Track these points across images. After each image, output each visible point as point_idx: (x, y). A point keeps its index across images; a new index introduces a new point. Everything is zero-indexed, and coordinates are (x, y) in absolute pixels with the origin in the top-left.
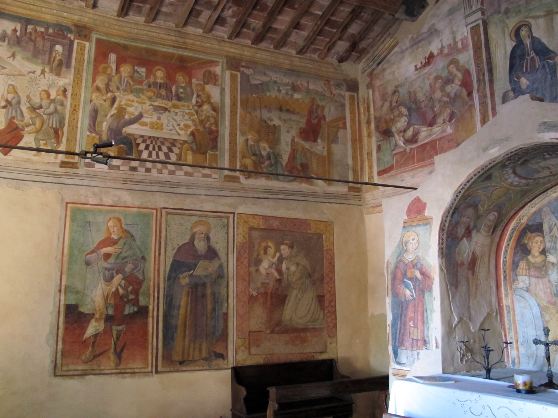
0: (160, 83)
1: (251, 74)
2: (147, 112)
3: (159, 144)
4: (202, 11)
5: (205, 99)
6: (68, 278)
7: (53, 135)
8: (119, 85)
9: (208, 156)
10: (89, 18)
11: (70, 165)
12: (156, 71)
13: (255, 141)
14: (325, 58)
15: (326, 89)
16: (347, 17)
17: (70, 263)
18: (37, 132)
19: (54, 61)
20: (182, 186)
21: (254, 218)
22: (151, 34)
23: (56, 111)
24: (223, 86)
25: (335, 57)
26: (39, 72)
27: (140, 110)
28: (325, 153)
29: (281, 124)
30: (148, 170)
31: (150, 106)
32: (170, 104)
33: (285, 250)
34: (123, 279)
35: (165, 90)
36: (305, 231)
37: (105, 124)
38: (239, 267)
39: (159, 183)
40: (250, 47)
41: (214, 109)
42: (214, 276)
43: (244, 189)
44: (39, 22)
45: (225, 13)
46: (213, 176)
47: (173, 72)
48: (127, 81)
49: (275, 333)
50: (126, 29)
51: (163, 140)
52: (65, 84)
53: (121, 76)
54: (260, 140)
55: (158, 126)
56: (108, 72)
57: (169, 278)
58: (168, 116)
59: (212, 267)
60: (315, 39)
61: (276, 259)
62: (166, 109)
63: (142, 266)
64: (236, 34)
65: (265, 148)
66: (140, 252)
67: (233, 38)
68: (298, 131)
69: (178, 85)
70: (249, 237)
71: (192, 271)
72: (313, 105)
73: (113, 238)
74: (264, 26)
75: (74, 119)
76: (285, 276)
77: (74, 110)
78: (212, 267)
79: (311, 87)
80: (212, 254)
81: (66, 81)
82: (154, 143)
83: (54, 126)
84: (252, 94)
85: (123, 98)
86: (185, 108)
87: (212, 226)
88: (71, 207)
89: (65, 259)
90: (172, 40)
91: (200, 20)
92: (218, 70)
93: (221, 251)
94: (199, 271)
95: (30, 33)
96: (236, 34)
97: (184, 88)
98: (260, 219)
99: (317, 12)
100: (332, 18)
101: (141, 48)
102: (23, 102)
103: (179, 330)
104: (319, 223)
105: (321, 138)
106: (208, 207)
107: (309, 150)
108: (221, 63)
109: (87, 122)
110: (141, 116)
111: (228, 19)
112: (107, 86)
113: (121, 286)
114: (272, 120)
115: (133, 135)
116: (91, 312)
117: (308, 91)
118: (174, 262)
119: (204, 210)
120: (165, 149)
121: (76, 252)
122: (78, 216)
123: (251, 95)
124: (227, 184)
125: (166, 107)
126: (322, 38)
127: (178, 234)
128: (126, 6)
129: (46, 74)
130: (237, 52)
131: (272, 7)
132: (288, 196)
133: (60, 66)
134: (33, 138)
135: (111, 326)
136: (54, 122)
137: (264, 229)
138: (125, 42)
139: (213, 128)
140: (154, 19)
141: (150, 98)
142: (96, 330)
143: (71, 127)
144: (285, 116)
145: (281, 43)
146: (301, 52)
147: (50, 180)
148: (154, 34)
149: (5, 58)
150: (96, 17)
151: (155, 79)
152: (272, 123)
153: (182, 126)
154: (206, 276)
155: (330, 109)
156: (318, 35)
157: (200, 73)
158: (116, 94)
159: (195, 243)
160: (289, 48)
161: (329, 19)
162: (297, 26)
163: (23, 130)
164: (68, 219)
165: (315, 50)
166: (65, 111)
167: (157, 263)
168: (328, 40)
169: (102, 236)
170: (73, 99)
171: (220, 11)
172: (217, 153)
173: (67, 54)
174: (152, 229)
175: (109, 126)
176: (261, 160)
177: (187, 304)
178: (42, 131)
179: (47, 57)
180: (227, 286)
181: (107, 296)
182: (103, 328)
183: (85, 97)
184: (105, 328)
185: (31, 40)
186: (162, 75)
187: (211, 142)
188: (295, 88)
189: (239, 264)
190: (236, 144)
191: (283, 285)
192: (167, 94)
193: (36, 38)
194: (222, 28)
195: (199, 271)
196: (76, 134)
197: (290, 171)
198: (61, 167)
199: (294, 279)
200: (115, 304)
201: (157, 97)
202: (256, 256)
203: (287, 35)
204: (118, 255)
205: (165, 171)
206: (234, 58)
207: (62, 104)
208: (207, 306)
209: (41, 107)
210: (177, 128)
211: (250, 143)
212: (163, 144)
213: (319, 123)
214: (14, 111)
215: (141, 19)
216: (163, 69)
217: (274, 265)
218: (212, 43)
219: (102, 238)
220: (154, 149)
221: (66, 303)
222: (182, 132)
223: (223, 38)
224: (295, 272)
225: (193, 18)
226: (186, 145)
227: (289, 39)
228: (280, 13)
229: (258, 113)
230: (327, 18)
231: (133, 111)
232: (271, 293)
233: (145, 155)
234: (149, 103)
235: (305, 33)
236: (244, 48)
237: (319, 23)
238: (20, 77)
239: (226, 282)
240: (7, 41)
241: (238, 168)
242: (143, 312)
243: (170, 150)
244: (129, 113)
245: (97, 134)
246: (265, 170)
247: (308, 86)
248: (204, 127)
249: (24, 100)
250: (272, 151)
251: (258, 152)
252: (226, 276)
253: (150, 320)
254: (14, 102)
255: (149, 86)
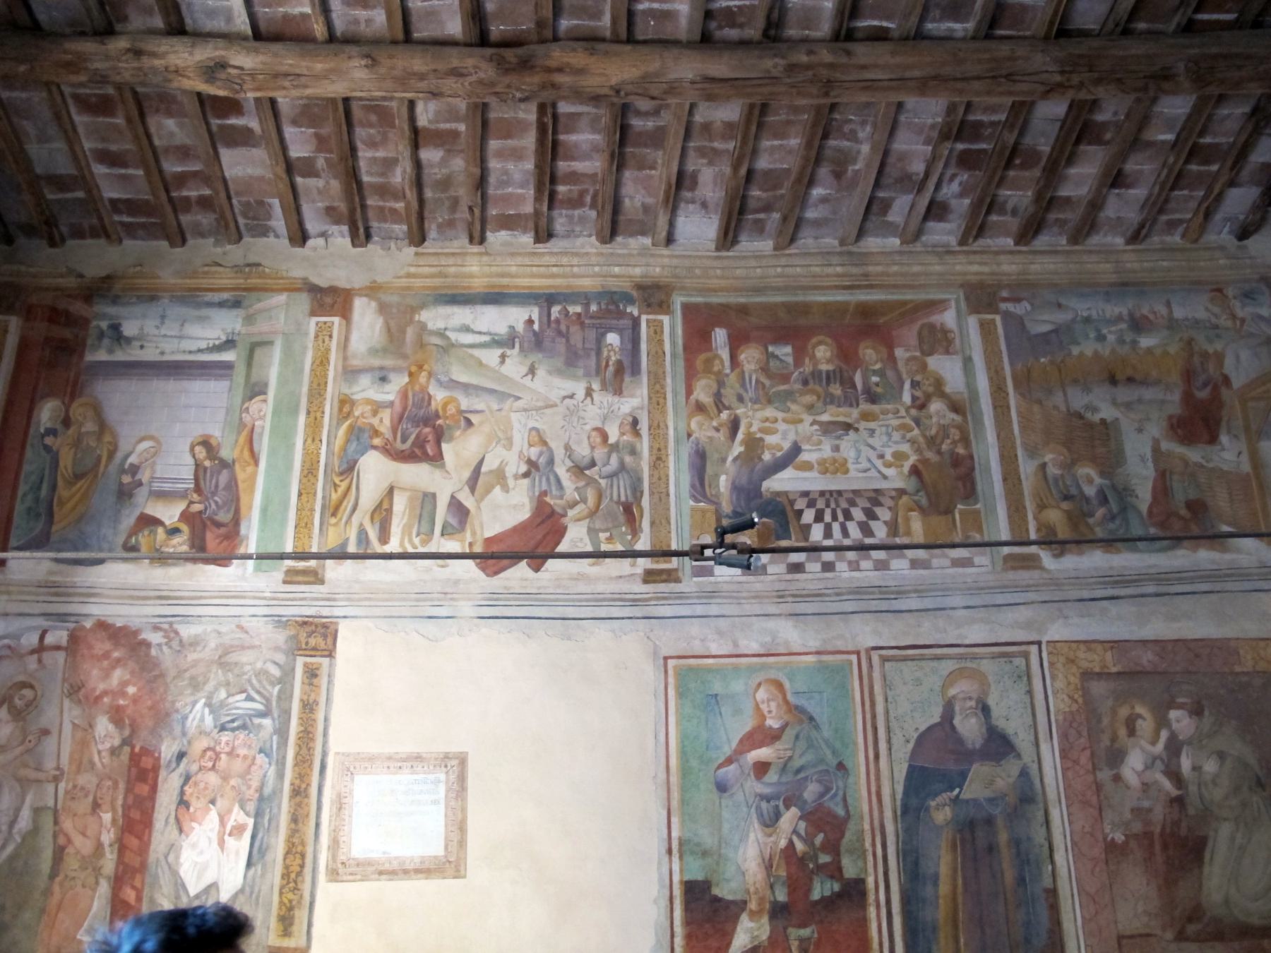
0: (828, 372)
1: (1027, 313)
2: (808, 439)
3: (844, 505)
4: (893, 199)
5: (931, 389)
6: (683, 822)
7: (622, 518)
8: (741, 391)
9: (957, 516)
10: (663, 267)
11: (664, 577)
12: (814, 347)
13: (1063, 466)
14: (1200, 236)
15: (1216, 310)
16: (1242, 128)
17: (683, 789)
18: (592, 514)
19: (607, 365)
20: (909, 592)
21: (1089, 649)
22: (789, 271)
23: (623, 466)
24: (968, 353)
25: (1226, 229)
26: (581, 393)
27: (792, 437)
28: (1246, 467)
29: (1119, 415)
30: (828, 567)
31: (812, 424)
32: (855, 413)
33: (1180, 720)
34: (800, 818)
35: (840, 384)
36: (1226, 670)
37: (723, 478)
38: (1070, 774)
39: (858, 593)
40: (1011, 252)
41: (956, 407)
42: (1012, 799)
43: (1055, 583)
44: (573, 294)
45: (944, 190)
46: (977, 560)
47: (849, 343)
48: (757, 381)
49: (1187, 939)
50: (738, 272)
51: (851, 495)
52: (634, 409)
53: (743, 372)
54: (1073, 463)
55: (836, 467)
56: (716, 369)
57: (906, 809)
58: (856, 442)
59: (1004, 776)
60: (1166, 201)
61: (1160, 747)
62: (848, 427)
63: (841, 784)
64: (976, 229)
65: (1089, 479)
66: (834, 753)
67: (971, 240)
68: (1164, 424)
69: (867, 369)
70: (1083, 696)
71: (957, 790)
72: (1191, 355)
73: (771, 728)
74: (1038, 197)
75: (660, 479)
76: (1193, 789)
77: (659, 460)
78: (1004, 776)
79: (1178, 313)
80: (998, 745)
81: (635, 402)
82: (833, 505)
83: (623, 499)
84: (1037, 359)
85: (753, 418)
86: (890, 416)
87: (990, 678)
88: (675, 667)
89: (674, 779)
90: (838, 275)
91: (890, 218)
92: (948, 318)
93: (1022, 735)
94: (973, 790)
95: (558, 321)
96: (976, 229)
97: (881, 373)
98: (1105, 651)
99: (1162, 137)
100: (1202, 140)
101: (776, 305)
102: (557, 460)
103: (942, 935)
104: (1262, 644)
105: (1229, 432)
106: (976, 634)
107: (1202, 466)
108: (953, 303)
109: (686, 479)
110: (796, 450)
111: (953, 202)
112: (718, 397)
113: (799, 836)
114: (1095, 410)
115: (786, 493)
116: (738, 897)
117: (1172, 325)
118: (912, 769)
119: (967, 642)
120: (858, 514)
121: (694, 763)
122: (691, 682)
123: (1037, 363)
124: (1011, 575)
125: (848, 420)
126: (1185, 192)
127: (914, 705)
128: (733, 225)
129: (595, 395)
130: (986, 269)
131: (1051, 154)
132: (1165, 587)
133: (618, 376)
134: (585, 530)
135: (785, 929)
136: (621, 490)
137: (1119, 673)
138: (742, 300)
139: (961, 450)
140: (792, 240)
141: (810, 408)
142: (754, 938)
143: (656, 496)
144: (1124, 394)
145: (1087, 226)
146: (1136, 237)
147: (627, 612)
148: (798, 269)
149: (518, 378)
150: (675, 262)
151: (815, 364)
152: (1096, 418)
153: (888, 457)
154: (991, 800)
155: (1238, 357)
156: (1172, 189)
157: (910, 334)
158: (738, 412)
159: (956, 722)
160: (1105, 235)
161: (1195, 145)
162: (1116, 179)
163: (565, 515)
164: (671, 692)
165: (1172, 225)
166: (639, 465)
167: (872, 777)
168: (1202, 193)
169: (746, 724)
170: (653, 437)
171: (932, 188)
172: (978, 506)
173: (630, 346)
174: (853, 699)
175: (733, 483)
176: (1085, 509)
177: (955, 870)
178: (600, 513)
179: (592, 362)
180: (1047, 822)
181: (770, 859)
182: (768, 933)
183: (675, 429)
184: (771, 932)
185: (560, 333)
186: (828, 354)
187: (960, 484)
188: (1138, 325)
189: (1070, 764)
190: (1020, 480)
191: (1191, 811)
192: (844, 392)
193: (568, 327)
194: (942, 225)
195: (973, 790)
196: (669, 509)
197: (1162, 525)
198: (646, 582)
199: (1218, 794)
200: (789, 877)
201: (825, 404)
202: (1108, 743)
203: (1095, 205)
204: (785, 765)
205: (865, 564)
206: (981, 286)
207: (633, 452)
208: (1002, 874)
209: (593, 464)
210: (879, 463)
211: (1053, 471)
212: (853, 503)
213: (1216, 399)
214: (544, 479)
215: (766, 245)
216: (829, 340)
217: (1158, 762)
218: (926, 262)
219: (748, 728)
220: (835, 518)
221: (686, 878)
222: (890, 472)
223: (948, 245)
224: (1217, 776)
225: (874, 218)
226: (905, 498)
227: (1102, 215)
228: (1070, 161)
229: (1058, 399)
230: (1190, 144)
231: (778, 441)
232: (1162, 834)
233: (817, 534)
234: (811, 419)
235: (1138, 193)
236: (1000, 258)
237: (1171, 160)
238: (548, 411)
239: (1042, 812)
240: (517, 345)
241: (1033, 536)
242: (854, 892)
243: (871, 515)
244: (771, 447)
245: (710, 501)
246: (1100, 533)
247: (1171, 312)
248: (939, 452)
249: (559, 453)
250: (1107, 482)
251: (1074, 491)
252: (1040, 798)
253: (872, 912)
254: (542, 461)
255: (805, 383)
